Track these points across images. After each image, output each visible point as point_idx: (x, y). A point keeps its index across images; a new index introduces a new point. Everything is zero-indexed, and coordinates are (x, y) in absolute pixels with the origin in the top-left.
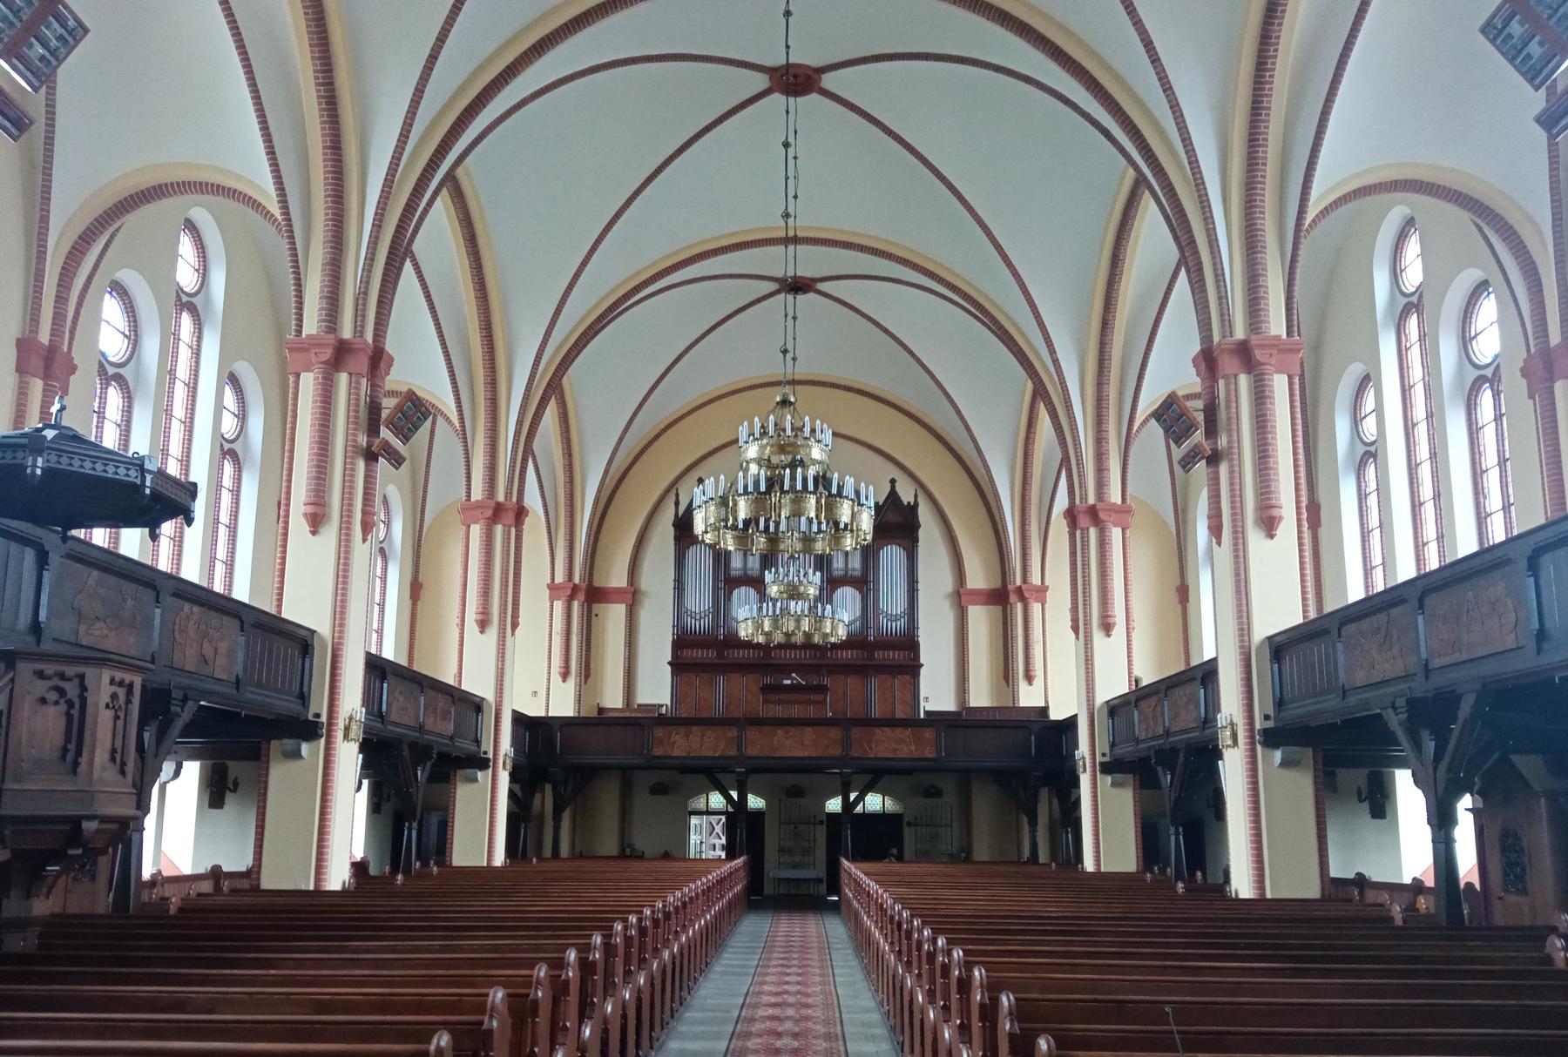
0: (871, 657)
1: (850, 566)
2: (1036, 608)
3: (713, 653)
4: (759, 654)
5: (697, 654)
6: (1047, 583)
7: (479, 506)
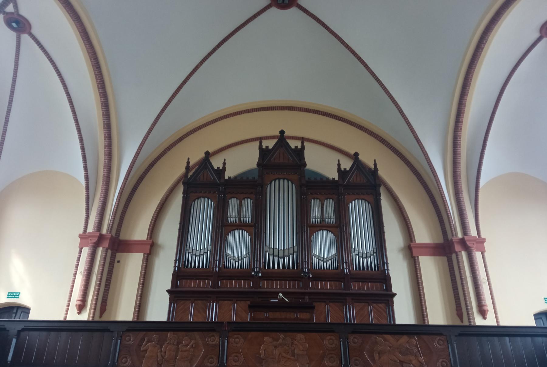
0: (348, 287)
1: (325, 215)
2: (478, 255)
3: (208, 284)
4: (249, 284)
5: (194, 285)
6: (483, 236)
7: (91, 235)
